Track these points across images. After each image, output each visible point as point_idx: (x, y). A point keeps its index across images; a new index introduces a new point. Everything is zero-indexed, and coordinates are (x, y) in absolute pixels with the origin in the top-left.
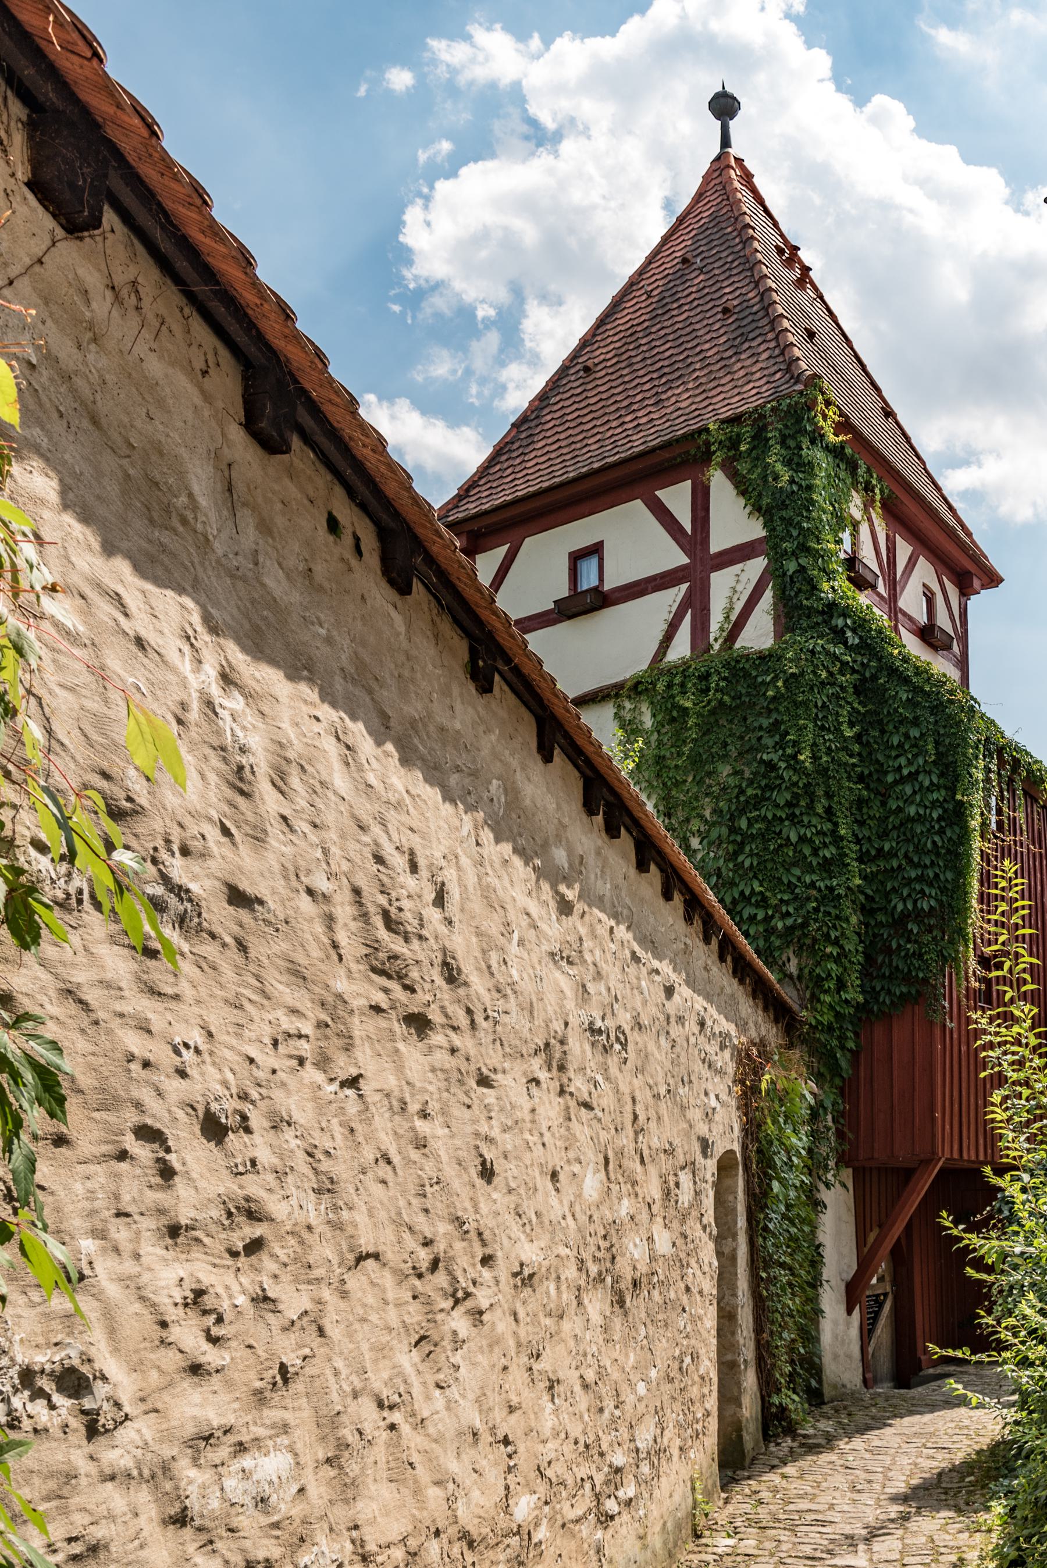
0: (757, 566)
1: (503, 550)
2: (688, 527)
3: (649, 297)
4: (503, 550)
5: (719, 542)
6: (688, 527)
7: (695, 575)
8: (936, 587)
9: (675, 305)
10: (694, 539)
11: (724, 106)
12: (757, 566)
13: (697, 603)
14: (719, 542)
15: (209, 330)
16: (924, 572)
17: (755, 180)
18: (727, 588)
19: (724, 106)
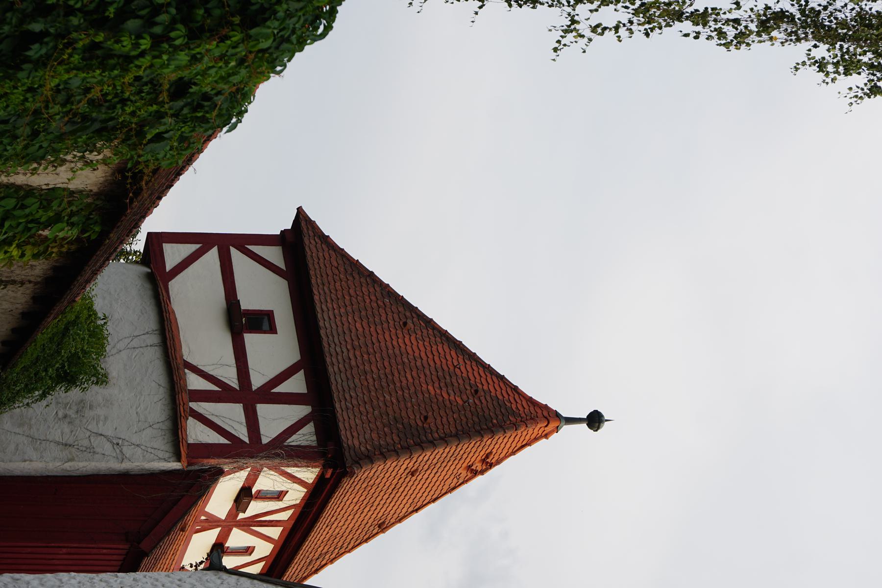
0: (243, 434)
1: (281, 264)
2: (275, 390)
3: (455, 367)
4: (281, 264)
5: (263, 410)
6: (275, 390)
7: (248, 396)
8: (255, 556)
9: (400, 393)
10: (268, 394)
11: (595, 420)
12: (243, 434)
13: (224, 394)
14: (263, 410)
15: (33, 473)
16: (264, 549)
17: (544, 440)
18: (231, 416)
19: (595, 420)
